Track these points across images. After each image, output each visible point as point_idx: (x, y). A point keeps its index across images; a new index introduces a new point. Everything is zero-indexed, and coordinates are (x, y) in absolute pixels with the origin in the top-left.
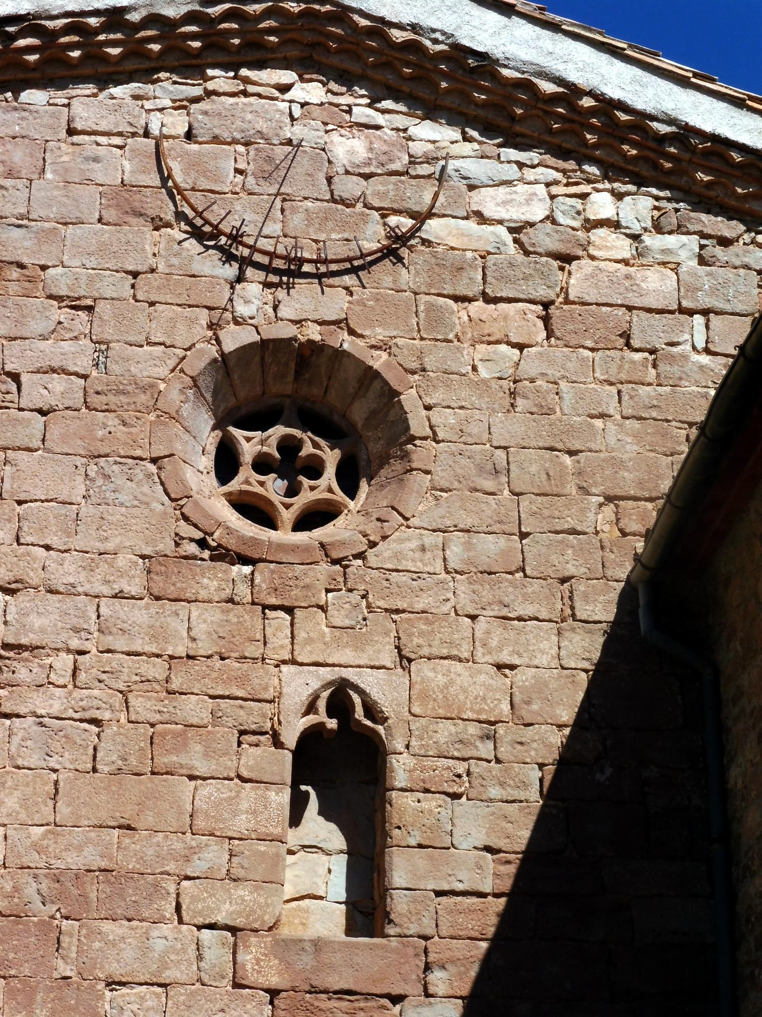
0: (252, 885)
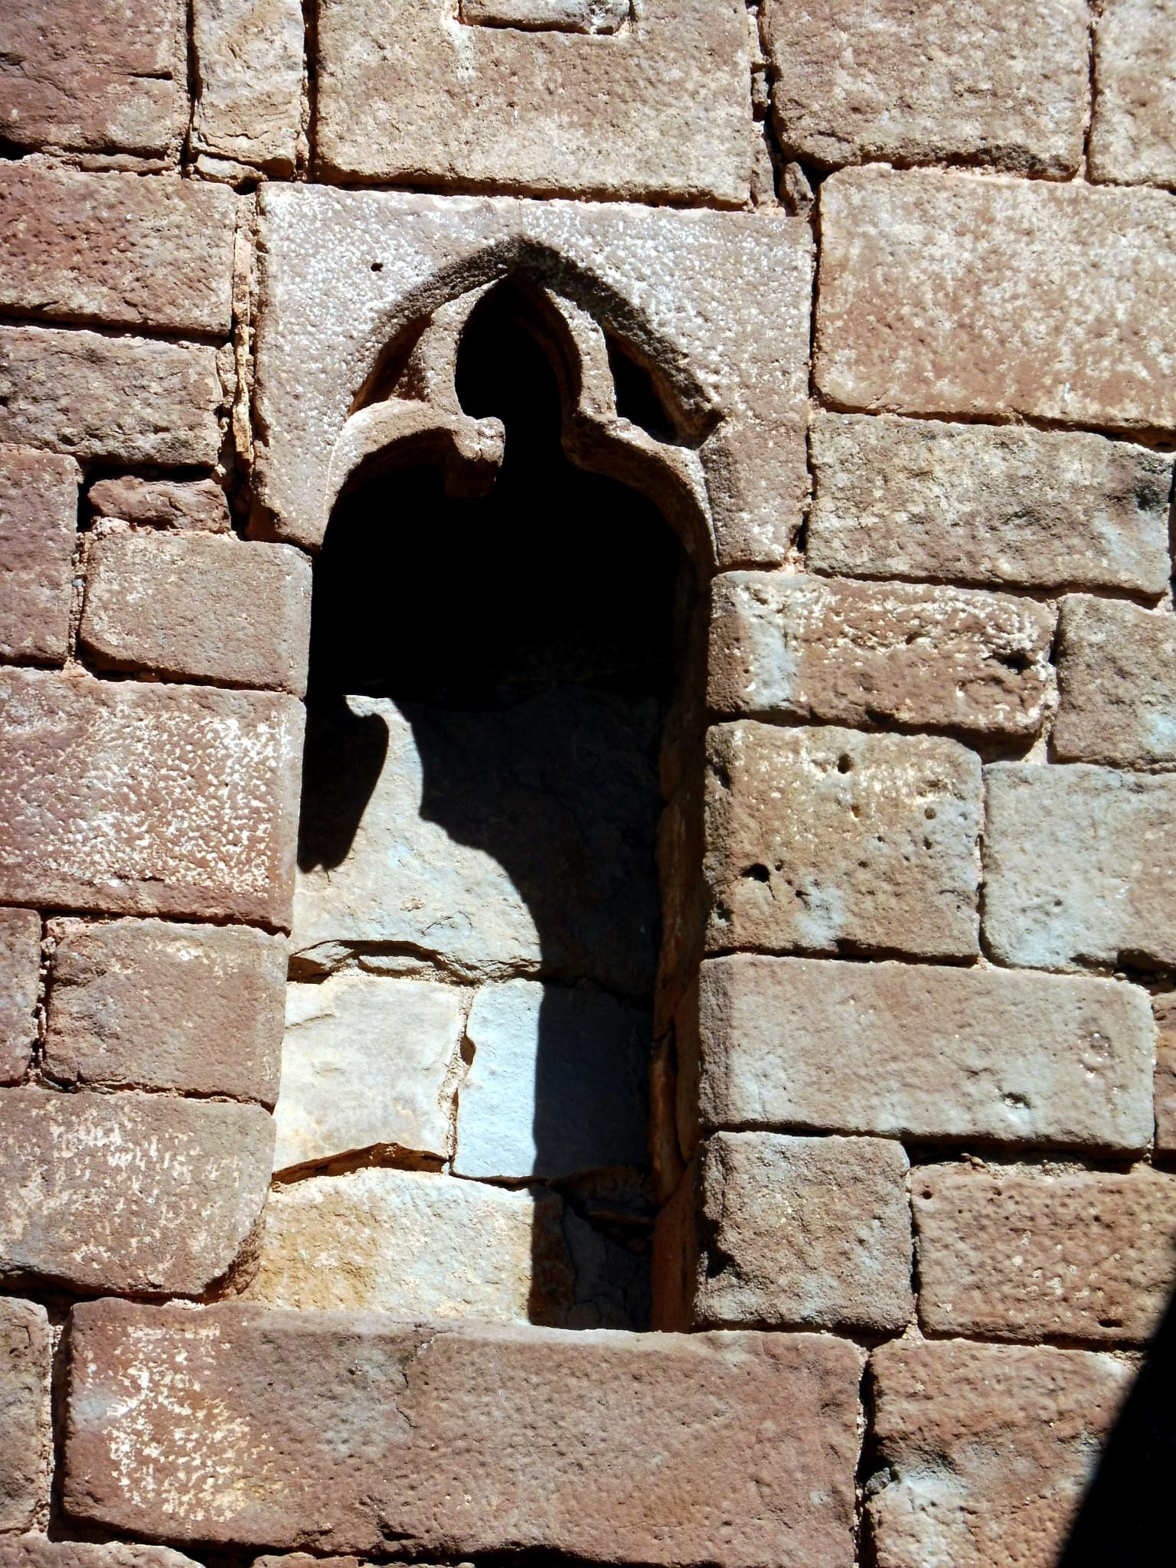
0: (138, 1106)
